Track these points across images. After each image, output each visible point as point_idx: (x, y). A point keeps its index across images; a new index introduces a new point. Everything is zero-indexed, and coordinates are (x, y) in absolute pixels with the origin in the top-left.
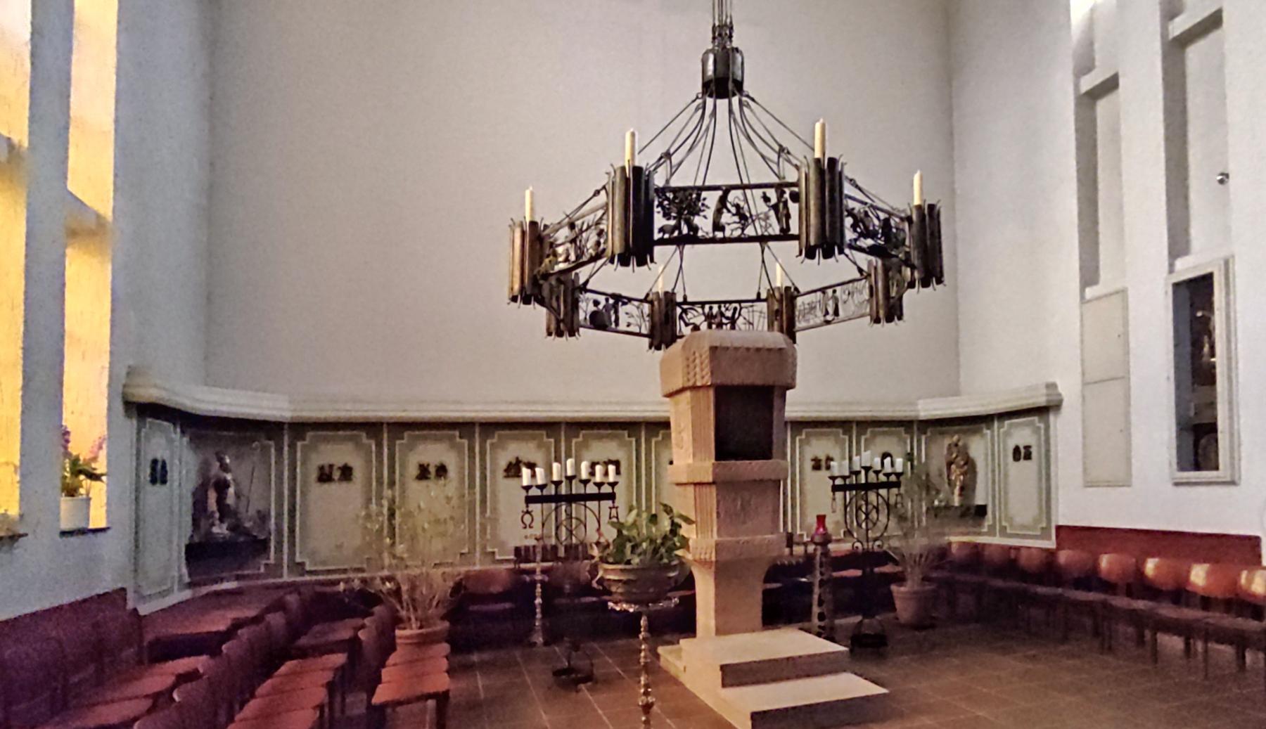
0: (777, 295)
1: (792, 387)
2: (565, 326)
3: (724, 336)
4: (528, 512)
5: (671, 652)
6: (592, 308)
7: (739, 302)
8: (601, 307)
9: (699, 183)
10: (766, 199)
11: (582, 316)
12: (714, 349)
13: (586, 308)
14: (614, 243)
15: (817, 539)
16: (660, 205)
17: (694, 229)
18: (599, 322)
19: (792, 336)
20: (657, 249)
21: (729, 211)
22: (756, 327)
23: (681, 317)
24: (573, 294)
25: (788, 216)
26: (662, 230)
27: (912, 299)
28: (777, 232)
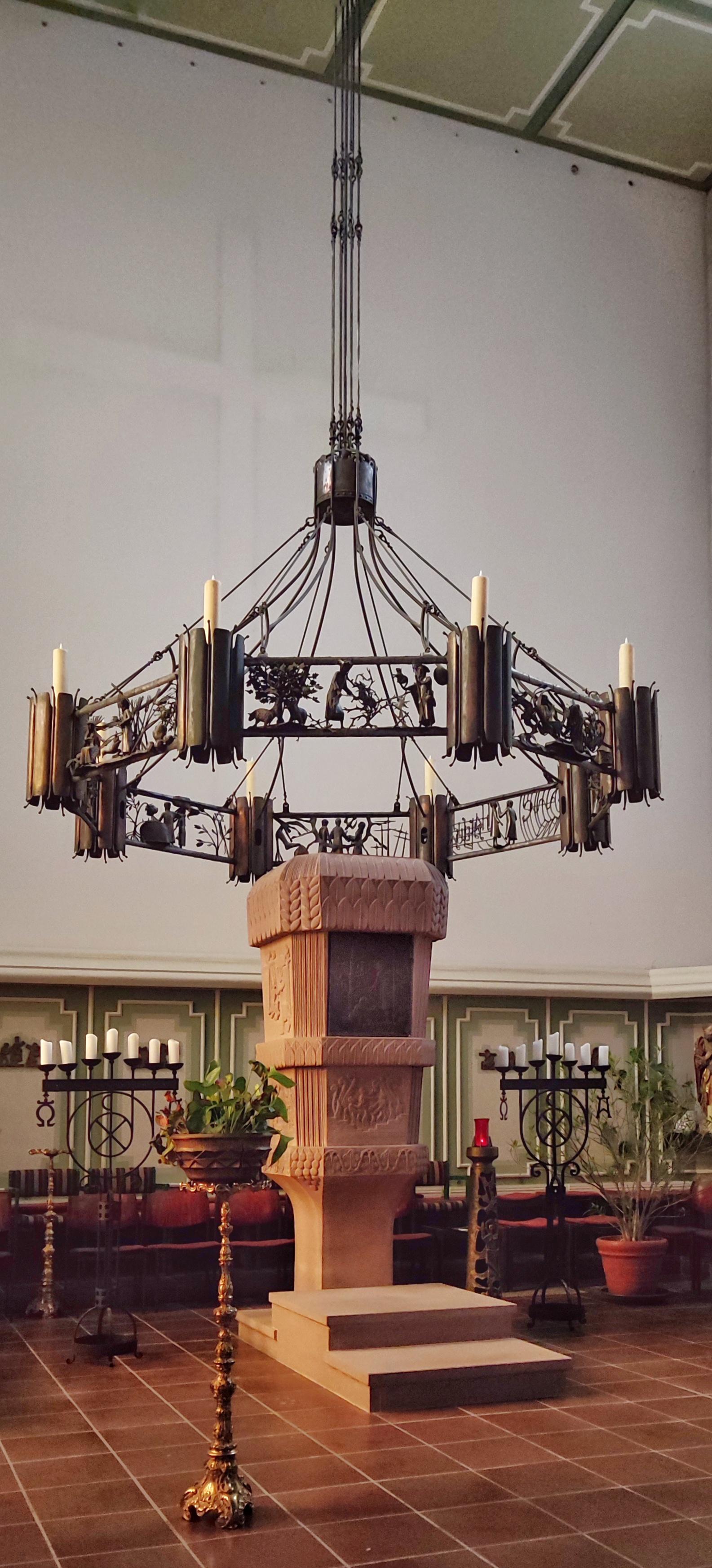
0: (424, 806)
1: (441, 937)
2: (103, 841)
3: (347, 862)
4: (46, 1103)
5: (250, 1316)
6: (144, 817)
7: (369, 816)
8: (158, 816)
9: (306, 654)
10: (402, 679)
11: (129, 828)
12: (326, 881)
13: (135, 817)
14: (186, 728)
15: (476, 1152)
16: (253, 681)
17: (302, 716)
18: (155, 837)
19: (446, 869)
20: (246, 740)
21: (349, 693)
22: (393, 851)
23: (279, 835)
24: (116, 795)
25: (432, 703)
26: (252, 716)
27: (622, 816)
28: (417, 724)
